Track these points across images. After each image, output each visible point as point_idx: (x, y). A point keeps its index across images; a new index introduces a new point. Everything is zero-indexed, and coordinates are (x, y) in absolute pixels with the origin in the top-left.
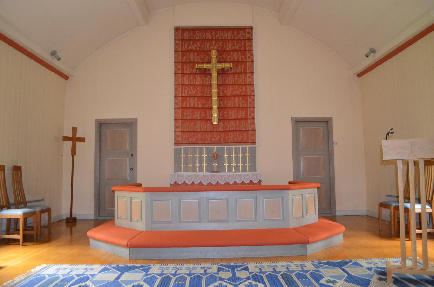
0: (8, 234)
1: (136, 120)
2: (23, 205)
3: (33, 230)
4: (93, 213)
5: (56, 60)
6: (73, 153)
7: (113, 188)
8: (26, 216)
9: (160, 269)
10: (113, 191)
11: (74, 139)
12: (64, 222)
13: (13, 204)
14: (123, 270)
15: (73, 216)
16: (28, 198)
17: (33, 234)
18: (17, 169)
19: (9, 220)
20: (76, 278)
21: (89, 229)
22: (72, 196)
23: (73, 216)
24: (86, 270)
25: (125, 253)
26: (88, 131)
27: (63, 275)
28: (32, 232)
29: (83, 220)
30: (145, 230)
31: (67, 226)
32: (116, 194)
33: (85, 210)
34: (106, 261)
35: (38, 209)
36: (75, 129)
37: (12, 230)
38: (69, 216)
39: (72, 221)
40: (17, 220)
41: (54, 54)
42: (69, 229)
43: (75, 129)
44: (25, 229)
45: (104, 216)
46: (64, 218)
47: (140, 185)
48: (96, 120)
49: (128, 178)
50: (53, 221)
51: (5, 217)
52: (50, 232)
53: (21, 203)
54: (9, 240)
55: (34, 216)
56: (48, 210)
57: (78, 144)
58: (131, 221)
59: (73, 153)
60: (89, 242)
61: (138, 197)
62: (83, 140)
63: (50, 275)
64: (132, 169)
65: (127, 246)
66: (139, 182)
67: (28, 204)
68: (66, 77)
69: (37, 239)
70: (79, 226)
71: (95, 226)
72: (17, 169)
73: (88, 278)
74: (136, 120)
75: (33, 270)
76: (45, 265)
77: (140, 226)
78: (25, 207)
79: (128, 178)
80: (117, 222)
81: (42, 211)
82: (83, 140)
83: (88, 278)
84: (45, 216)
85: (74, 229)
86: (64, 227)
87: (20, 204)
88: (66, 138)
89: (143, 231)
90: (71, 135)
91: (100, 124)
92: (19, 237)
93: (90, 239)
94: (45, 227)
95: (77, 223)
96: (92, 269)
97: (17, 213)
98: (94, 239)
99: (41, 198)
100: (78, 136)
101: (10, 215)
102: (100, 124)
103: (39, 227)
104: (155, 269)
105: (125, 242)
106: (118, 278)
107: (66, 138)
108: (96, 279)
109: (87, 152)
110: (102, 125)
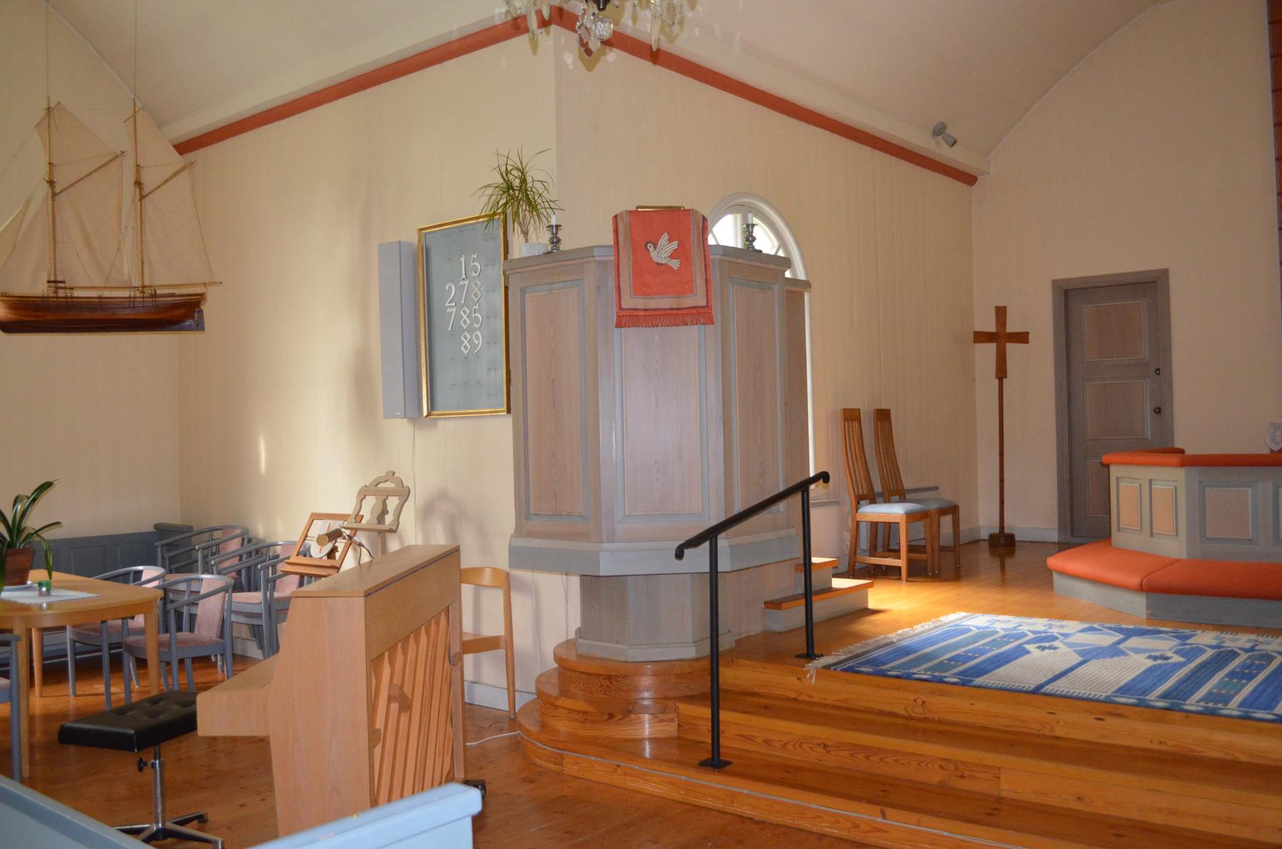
0: (872, 555)
1: (1165, 273)
2: (897, 498)
3: (925, 552)
4: (1054, 524)
5: (945, 146)
6: (1001, 373)
7: (1105, 459)
8: (911, 516)
9: (1217, 638)
10: (1107, 466)
11: (1002, 337)
12: (985, 546)
13: (881, 495)
14: (1128, 634)
15: (1007, 531)
16: (908, 483)
17: (926, 562)
18: (883, 416)
19: (874, 525)
20: (1031, 636)
21: (1051, 555)
22: (1002, 480)
23: (1007, 531)
24: (1051, 626)
25: (1137, 604)
26: (1036, 314)
27: (1004, 630)
28: (924, 556)
29: (1032, 542)
30: (1184, 556)
31: (992, 554)
32: (1115, 471)
33: (1035, 515)
34: (1092, 618)
35: (933, 506)
36: (1001, 313)
37: (879, 550)
38: (997, 531)
39: (1003, 544)
40: (890, 527)
41: (939, 131)
42: (997, 562)
43: (1001, 313)
44: (911, 549)
45: (1086, 521)
46: (985, 534)
47: (1182, 451)
48: (1055, 283)
49: (1149, 434)
50: (963, 540)
51: (868, 519)
52: (957, 560)
53: (895, 493)
54: (877, 566)
55: (928, 520)
56: (953, 510)
57: (1011, 347)
58: (1152, 535)
59: (1001, 373)
60: (1052, 582)
61: (1169, 480)
62: (1022, 338)
63: (978, 628)
64: (1158, 411)
65: (1141, 589)
66: (1178, 445)
67: (908, 496)
68: (969, 179)
69: (933, 572)
70: (1020, 555)
71: (1061, 550)
72: (883, 416)
73: (1055, 638)
74: (1165, 273)
75: (944, 619)
76: (964, 614)
77: (1174, 547)
78: (903, 500)
79: (1149, 434)
80: (1117, 538)
81: (943, 511)
82: (1022, 338)
83: (1055, 638)
84: (947, 521)
85: (1008, 562)
86: (984, 555)
87: (892, 493)
88: (981, 337)
89: (1178, 561)
90: (993, 329)
91: (1066, 291)
92: (901, 563)
93: (1055, 576)
94: (943, 549)
95: (1018, 552)
96: (1062, 627)
97: (894, 511)
98: (1064, 573)
99: (933, 485)
100: (1011, 328)
101: (884, 515)
102: (1066, 291)
103: (936, 548)
104: (1206, 638)
105: (1135, 580)
106: (1119, 643)
107: (981, 337)
108: (1072, 640)
109: (1035, 366)
110: (1070, 297)
